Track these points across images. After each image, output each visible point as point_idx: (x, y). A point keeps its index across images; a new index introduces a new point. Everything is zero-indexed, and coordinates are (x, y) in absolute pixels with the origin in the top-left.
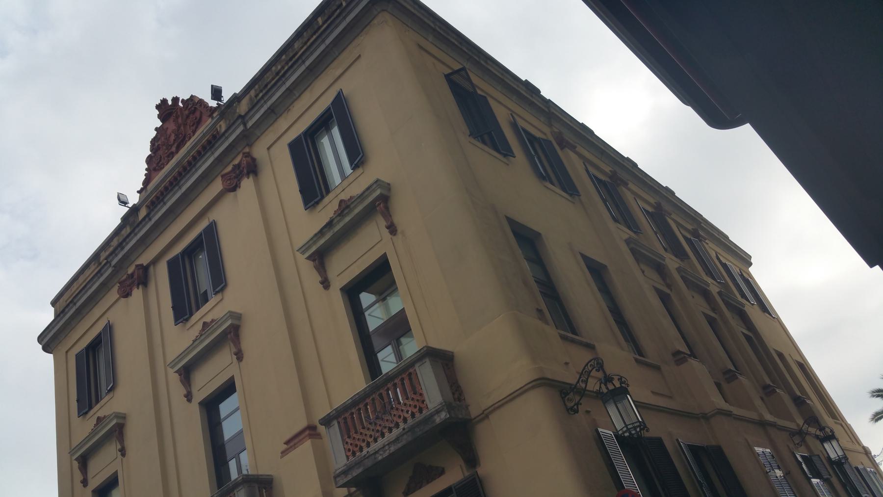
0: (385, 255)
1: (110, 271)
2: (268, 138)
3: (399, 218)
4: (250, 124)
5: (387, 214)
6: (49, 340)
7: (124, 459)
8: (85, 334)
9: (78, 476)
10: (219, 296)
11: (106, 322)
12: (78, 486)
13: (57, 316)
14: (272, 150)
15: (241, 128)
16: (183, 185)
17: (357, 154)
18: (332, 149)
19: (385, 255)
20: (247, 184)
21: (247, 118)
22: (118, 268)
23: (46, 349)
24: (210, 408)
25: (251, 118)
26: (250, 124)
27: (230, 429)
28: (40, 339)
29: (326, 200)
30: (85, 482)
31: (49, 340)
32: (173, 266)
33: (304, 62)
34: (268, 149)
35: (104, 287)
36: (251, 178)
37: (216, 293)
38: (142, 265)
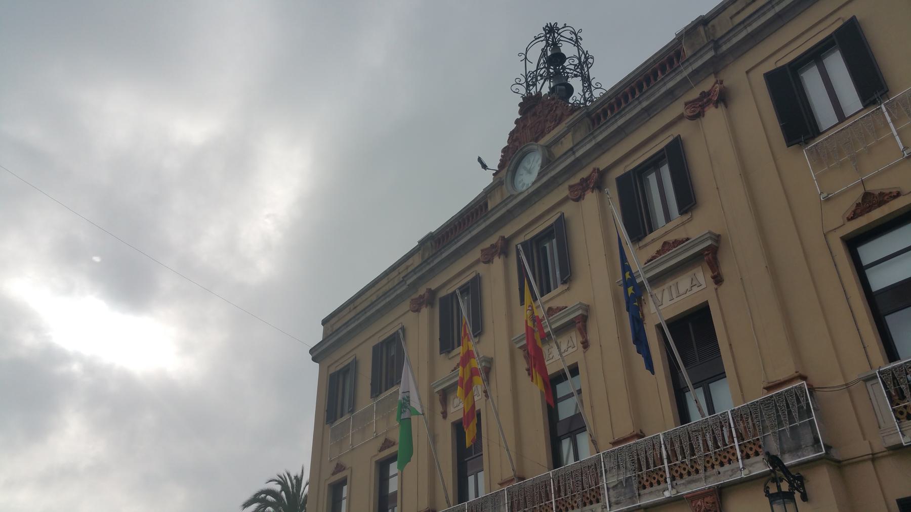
0: (577, 363)
1: (404, 288)
2: (750, 60)
3: (592, 335)
4: (724, 48)
5: (584, 331)
6: (317, 354)
7: (723, 288)
8: (370, 338)
9: (439, 408)
10: (565, 287)
11: (474, 275)
12: (439, 417)
13: (326, 338)
14: (751, 74)
15: (711, 54)
16: (598, 135)
17: (688, 200)
18: (660, 188)
19: (577, 363)
20: (714, 115)
21: (721, 42)
22: (414, 286)
23: (314, 359)
24: (383, 467)
25: (725, 43)
26: (724, 48)
27: (393, 486)
28: (311, 351)
29: (650, 237)
30: (445, 415)
31: (317, 354)
32: (622, 182)
33: (506, 205)
34: (747, 72)
35: (400, 299)
36: (502, 257)
37: (475, 336)
38: (430, 289)
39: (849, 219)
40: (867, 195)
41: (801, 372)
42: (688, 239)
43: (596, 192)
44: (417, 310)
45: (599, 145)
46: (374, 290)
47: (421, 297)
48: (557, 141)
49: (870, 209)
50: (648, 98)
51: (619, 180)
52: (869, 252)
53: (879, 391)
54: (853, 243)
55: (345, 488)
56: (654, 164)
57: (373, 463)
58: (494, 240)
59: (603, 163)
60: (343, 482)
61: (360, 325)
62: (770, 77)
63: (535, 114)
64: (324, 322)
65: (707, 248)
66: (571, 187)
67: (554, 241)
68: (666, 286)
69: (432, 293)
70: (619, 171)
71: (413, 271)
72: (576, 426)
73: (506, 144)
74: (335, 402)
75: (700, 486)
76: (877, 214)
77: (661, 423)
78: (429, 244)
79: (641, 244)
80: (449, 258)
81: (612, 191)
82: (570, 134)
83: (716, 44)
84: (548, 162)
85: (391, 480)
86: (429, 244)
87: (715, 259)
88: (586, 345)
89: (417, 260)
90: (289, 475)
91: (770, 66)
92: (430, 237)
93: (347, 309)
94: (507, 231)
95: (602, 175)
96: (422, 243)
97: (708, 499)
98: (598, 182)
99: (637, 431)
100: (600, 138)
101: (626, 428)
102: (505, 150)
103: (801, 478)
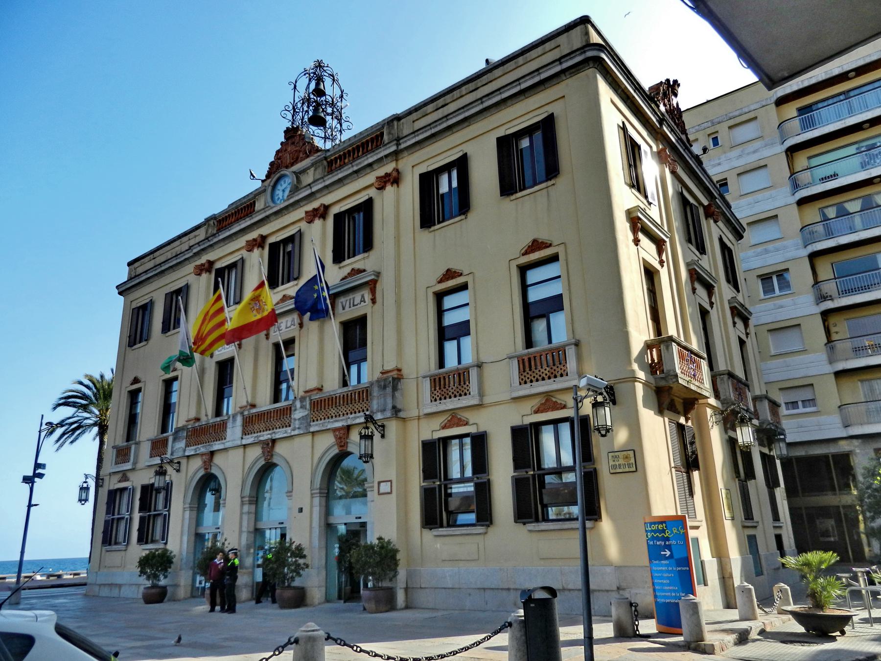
4: (402, 146)
5: (373, 291)
6: (123, 290)
13: (130, 279)
15: (394, 148)
20: (390, 189)
23: (120, 293)
31: (123, 290)
32: (338, 218)
39: (523, 255)
40: (535, 241)
41: (399, 366)
42: (364, 271)
43: (321, 220)
44: (199, 274)
45: (326, 187)
46: (168, 248)
47: (203, 265)
48: (304, 171)
49: (448, 279)
50: (357, 165)
51: (336, 216)
52: (533, 276)
53: (427, 384)
54: (523, 270)
55: (141, 395)
56: (446, 168)
57: (161, 382)
58: (315, 204)
59: (327, 200)
60: (175, 379)
61: (156, 275)
62: (500, 141)
63: (293, 143)
64: (129, 264)
65: (371, 281)
66: (306, 212)
67: (362, 214)
68: (348, 298)
69: (211, 263)
70: (335, 210)
71: (198, 243)
72: (463, 329)
73: (273, 159)
74: (136, 331)
75: (339, 424)
76: (451, 283)
77: (332, 385)
78: (211, 222)
79: (275, 291)
80: (224, 239)
81: (330, 221)
82: (313, 169)
83: (398, 140)
84: (295, 189)
85: (174, 394)
86: (211, 222)
87: (375, 287)
88: (374, 301)
89: (201, 234)
90: (81, 383)
91: (501, 132)
92: (213, 217)
93: (540, 50)
94: (264, 230)
95: (326, 208)
96: (207, 220)
97: (342, 432)
98: (321, 213)
99: (320, 387)
100: (327, 183)
101: (313, 384)
102: (272, 164)
103: (383, 426)
